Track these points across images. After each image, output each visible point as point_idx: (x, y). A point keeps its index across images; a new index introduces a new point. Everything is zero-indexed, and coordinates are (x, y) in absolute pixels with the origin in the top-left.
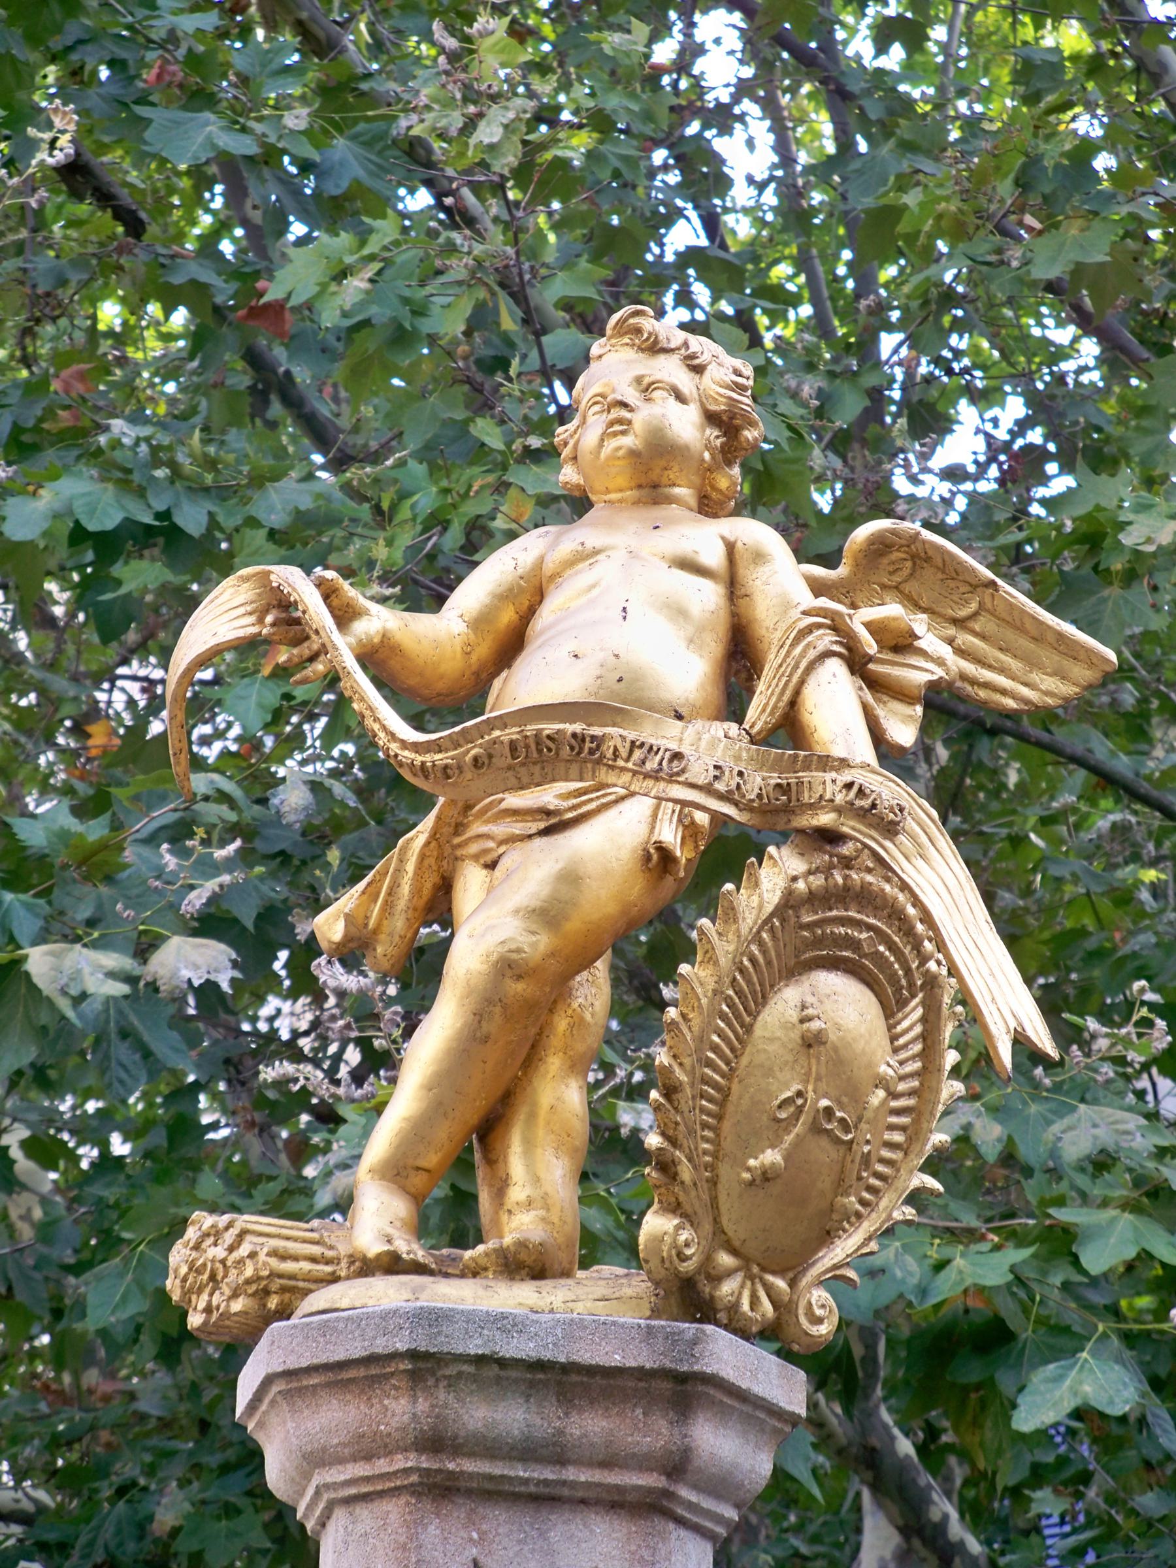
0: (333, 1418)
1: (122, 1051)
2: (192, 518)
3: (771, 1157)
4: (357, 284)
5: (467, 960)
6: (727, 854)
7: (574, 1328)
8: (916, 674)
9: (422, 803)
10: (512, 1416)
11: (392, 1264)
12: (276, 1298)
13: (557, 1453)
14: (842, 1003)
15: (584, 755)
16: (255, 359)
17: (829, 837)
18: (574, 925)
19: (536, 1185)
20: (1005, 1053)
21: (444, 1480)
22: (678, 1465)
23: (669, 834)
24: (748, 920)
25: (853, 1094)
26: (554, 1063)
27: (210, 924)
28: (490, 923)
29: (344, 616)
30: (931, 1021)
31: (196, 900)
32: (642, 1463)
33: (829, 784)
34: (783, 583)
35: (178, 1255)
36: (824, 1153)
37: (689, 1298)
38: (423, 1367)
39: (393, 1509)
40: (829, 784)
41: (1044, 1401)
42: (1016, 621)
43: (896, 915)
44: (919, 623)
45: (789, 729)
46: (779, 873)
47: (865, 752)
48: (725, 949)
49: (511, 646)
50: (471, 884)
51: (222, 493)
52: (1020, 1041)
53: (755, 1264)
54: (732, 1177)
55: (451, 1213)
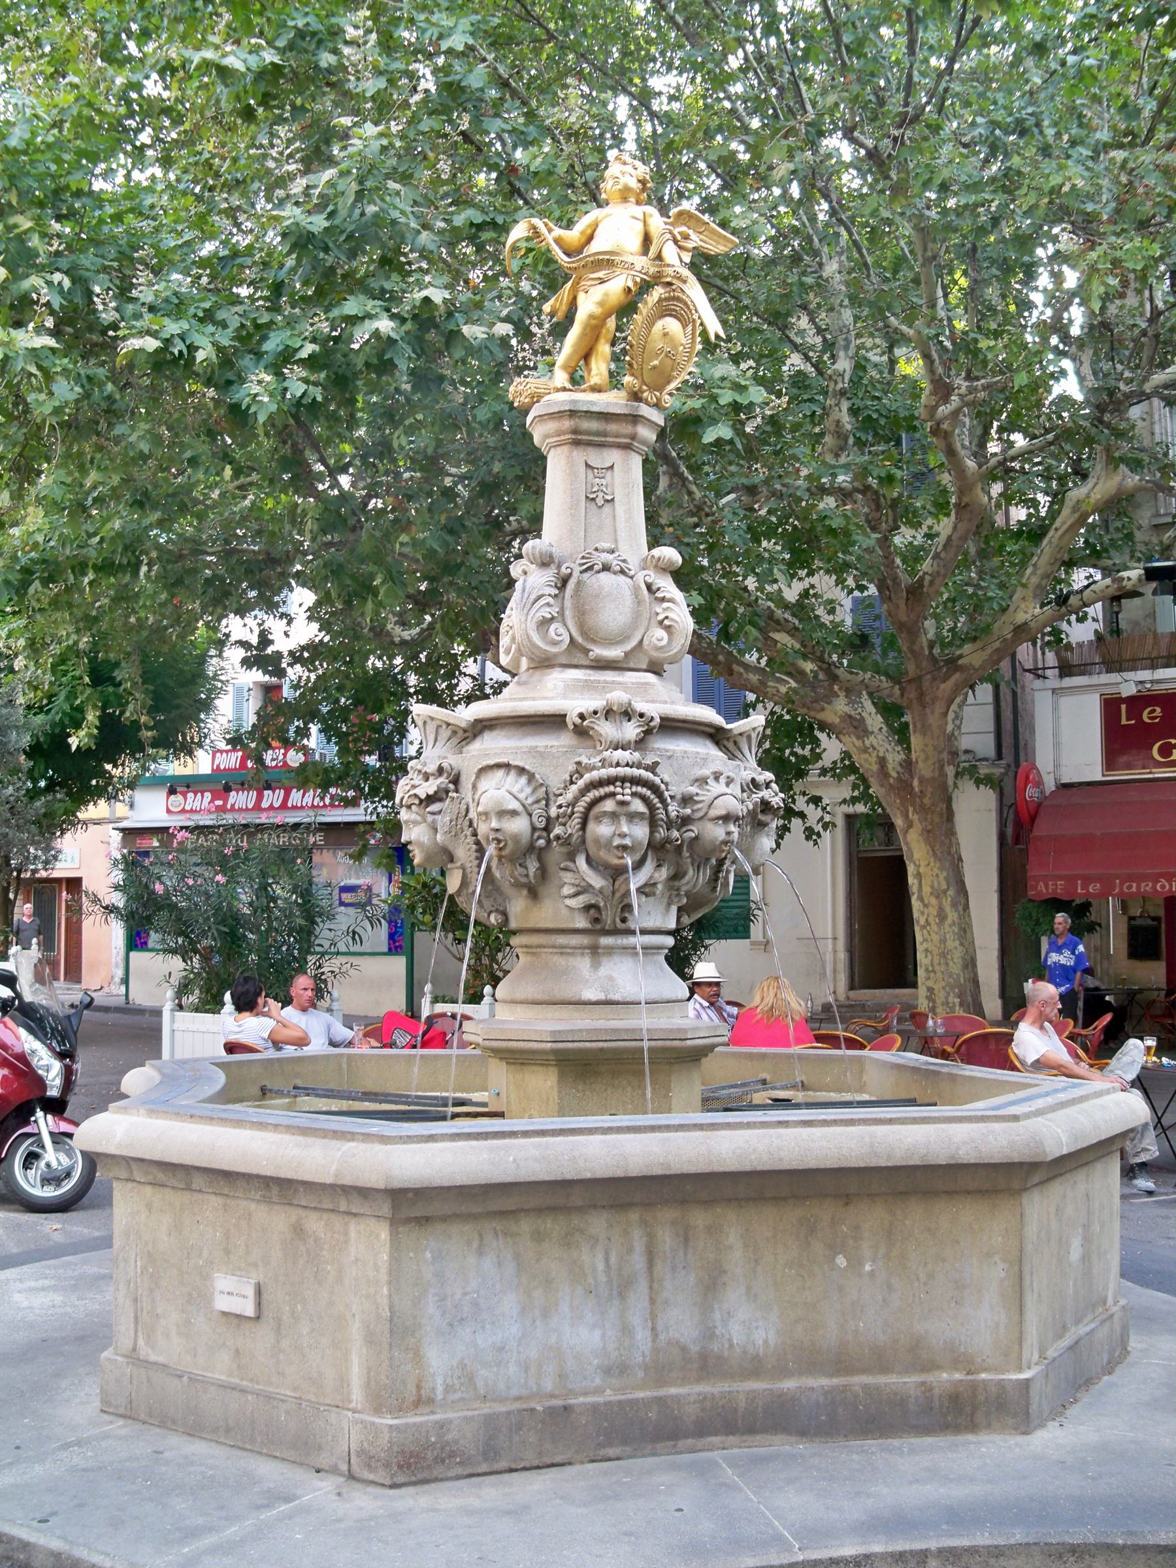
0: (551, 426)
1: (485, 352)
2: (500, 220)
3: (656, 362)
4: (539, 160)
5: (581, 317)
6: (645, 287)
7: (608, 404)
8: (690, 245)
9: (567, 278)
10: (594, 425)
11: (564, 389)
12: (536, 398)
13: (605, 434)
14: (672, 325)
15: (610, 264)
16: (510, 183)
17: (670, 284)
18: (607, 306)
19: (599, 369)
20: (713, 338)
21: (578, 441)
22: (633, 437)
23: (631, 284)
24: (650, 304)
25: (675, 347)
26: (602, 341)
27: (507, 319)
28: (588, 305)
29: (550, 231)
30: (694, 330)
31: (505, 313)
32: (625, 436)
33: (670, 271)
34: (657, 223)
35: (512, 389)
36: (668, 361)
37: (636, 397)
38: (573, 413)
39: (566, 448)
40: (670, 271)
41: (709, 436)
42: (714, 232)
43: (686, 304)
44: (691, 232)
45: (659, 257)
46: (658, 292)
47: (677, 263)
48: (645, 311)
49: (590, 238)
50: (581, 297)
51: (507, 213)
52: (717, 336)
53: (652, 388)
54: (647, 367)
55: (576, 381)
